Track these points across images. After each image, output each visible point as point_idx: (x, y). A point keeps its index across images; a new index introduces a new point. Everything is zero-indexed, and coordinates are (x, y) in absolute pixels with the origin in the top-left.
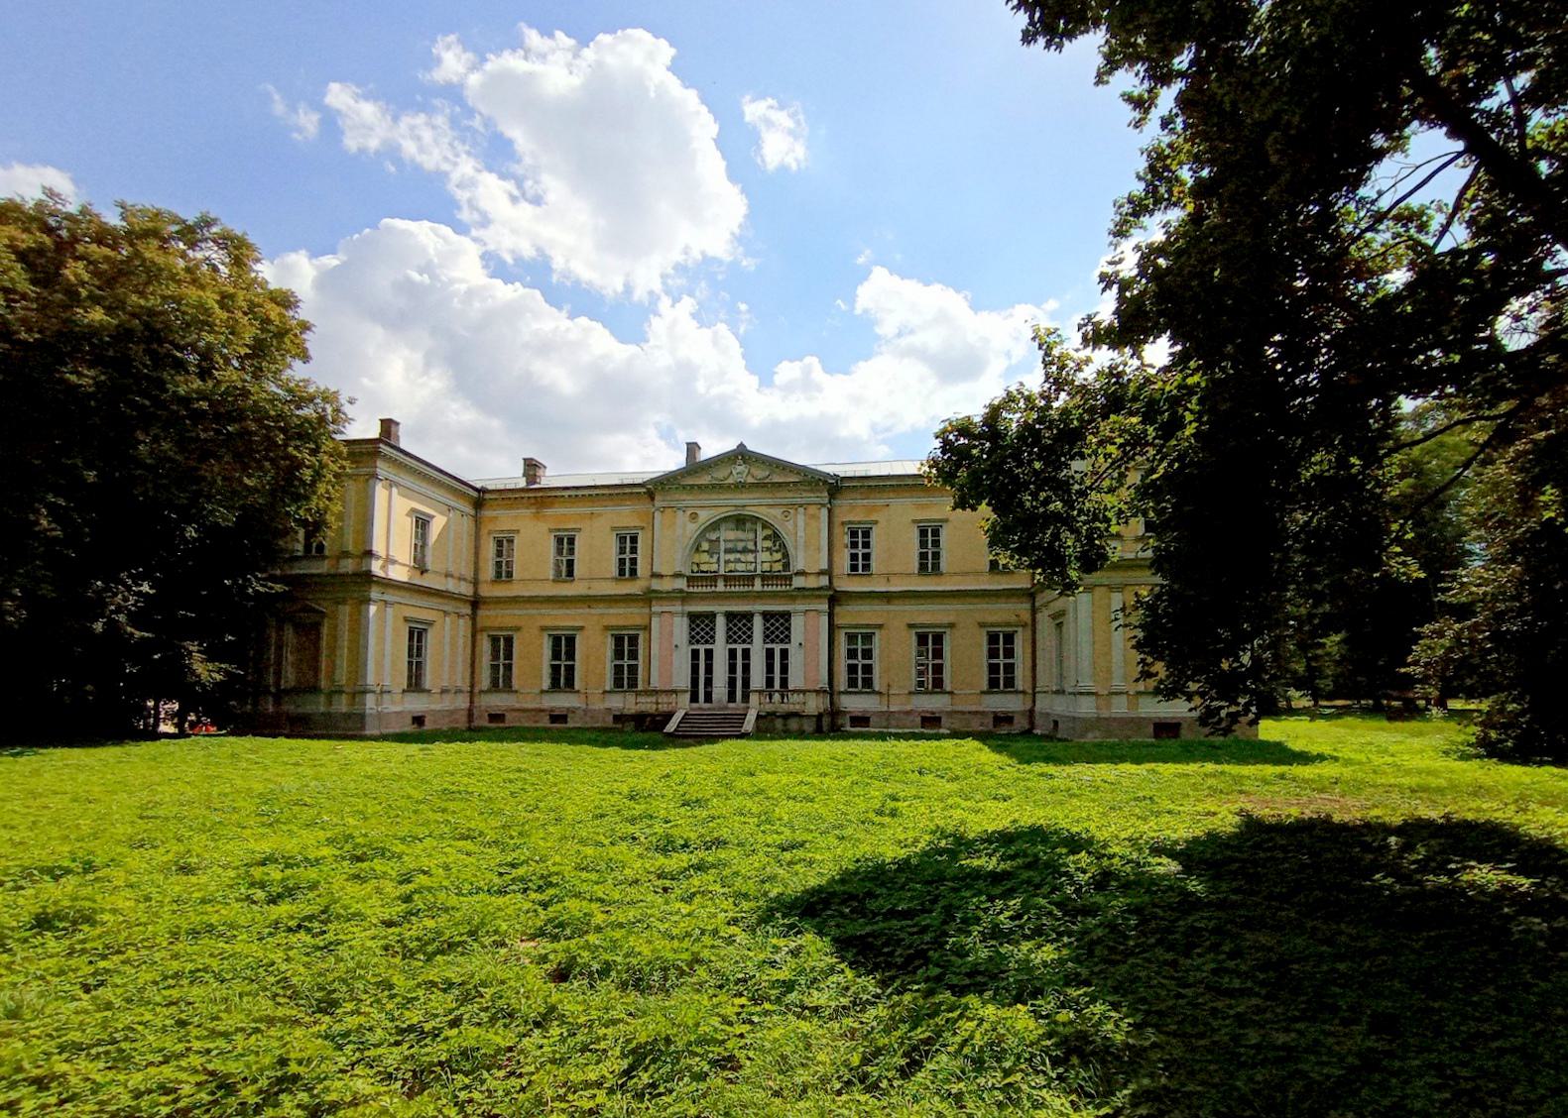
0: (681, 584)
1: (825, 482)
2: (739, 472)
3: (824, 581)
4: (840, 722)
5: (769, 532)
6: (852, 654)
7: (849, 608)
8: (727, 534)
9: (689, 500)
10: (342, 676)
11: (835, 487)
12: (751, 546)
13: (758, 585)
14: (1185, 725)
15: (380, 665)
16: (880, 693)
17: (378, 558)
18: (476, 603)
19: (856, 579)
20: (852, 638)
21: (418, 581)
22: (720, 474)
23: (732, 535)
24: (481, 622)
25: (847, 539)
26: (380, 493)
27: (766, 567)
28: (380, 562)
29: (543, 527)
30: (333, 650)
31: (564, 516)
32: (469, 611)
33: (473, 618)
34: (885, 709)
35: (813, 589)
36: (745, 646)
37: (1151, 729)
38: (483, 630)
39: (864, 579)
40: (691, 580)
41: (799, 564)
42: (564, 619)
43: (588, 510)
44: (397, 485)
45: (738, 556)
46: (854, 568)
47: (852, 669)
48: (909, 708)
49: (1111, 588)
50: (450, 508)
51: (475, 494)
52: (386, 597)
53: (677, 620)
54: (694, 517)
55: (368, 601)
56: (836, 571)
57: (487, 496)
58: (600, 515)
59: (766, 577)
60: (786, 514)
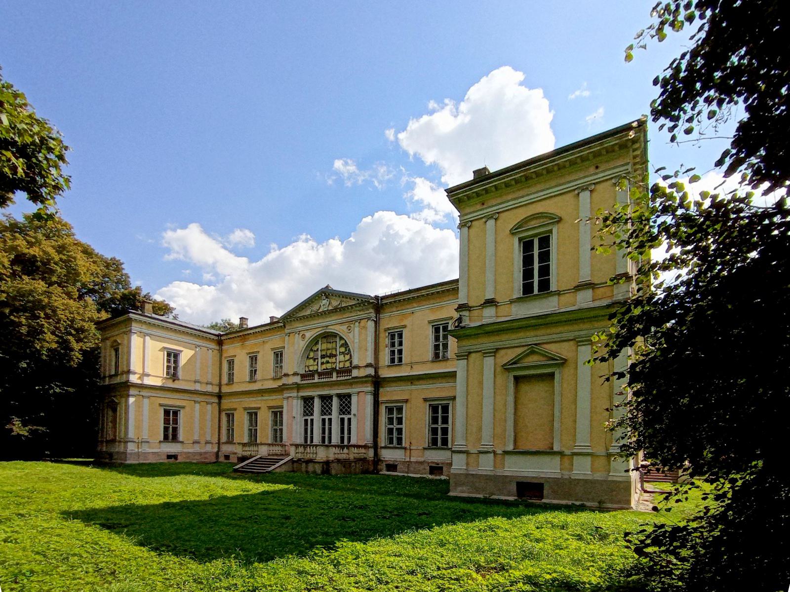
0: (297, 379)
1: (369, 303)
2: (324, 304)
3: (371, 371)
4: (379, 467)
5: (343, 342)
6: (391, 421)
7: (388, 389)
8: (322, 346)
9: (299, 326)
10: (122, 435)
11: (379, 305)
12: (334, 353)
13: (334, 378)
14: (546, 487)
15: (138, 427)
16: (405, 448)
17: (135, 373)
18: (220, 396)
19: (394, 368)
20: (390, 410)
21: (170, 384)
22: (315, 307)
23: (324, 346)
24: (224, 406)
25: (387, 341)
26: (136, 341)
27: (341, 365)
28: (137, 376)
29: (245, 351)
30: (120, 419)
31: (252, 344)
32: (217, 401)
33: (219, 404)
34: (408, 459)
35: (362, 377)
36: (330, 417)
37: (513, 487)
38: (224, 410)
39: (397, 367)
40: (303, 376)
41: (355, 362)
42: (252, 402)
43: (260, 340)
44: (148, 335)
45: (328, 359)
46: (393, 360)
47: (390, 431)
48: (422, 459)
49: (485, 353)
50: (197, 346)
51: (216, 338)
52: (141, 393)
53: (295, 401)
54: (303, 336)
55: (128, 396)
56: (381, 364)
57: (222, 338)
58: (267, 342)
59: (340, 372)
60: (349, 329)
